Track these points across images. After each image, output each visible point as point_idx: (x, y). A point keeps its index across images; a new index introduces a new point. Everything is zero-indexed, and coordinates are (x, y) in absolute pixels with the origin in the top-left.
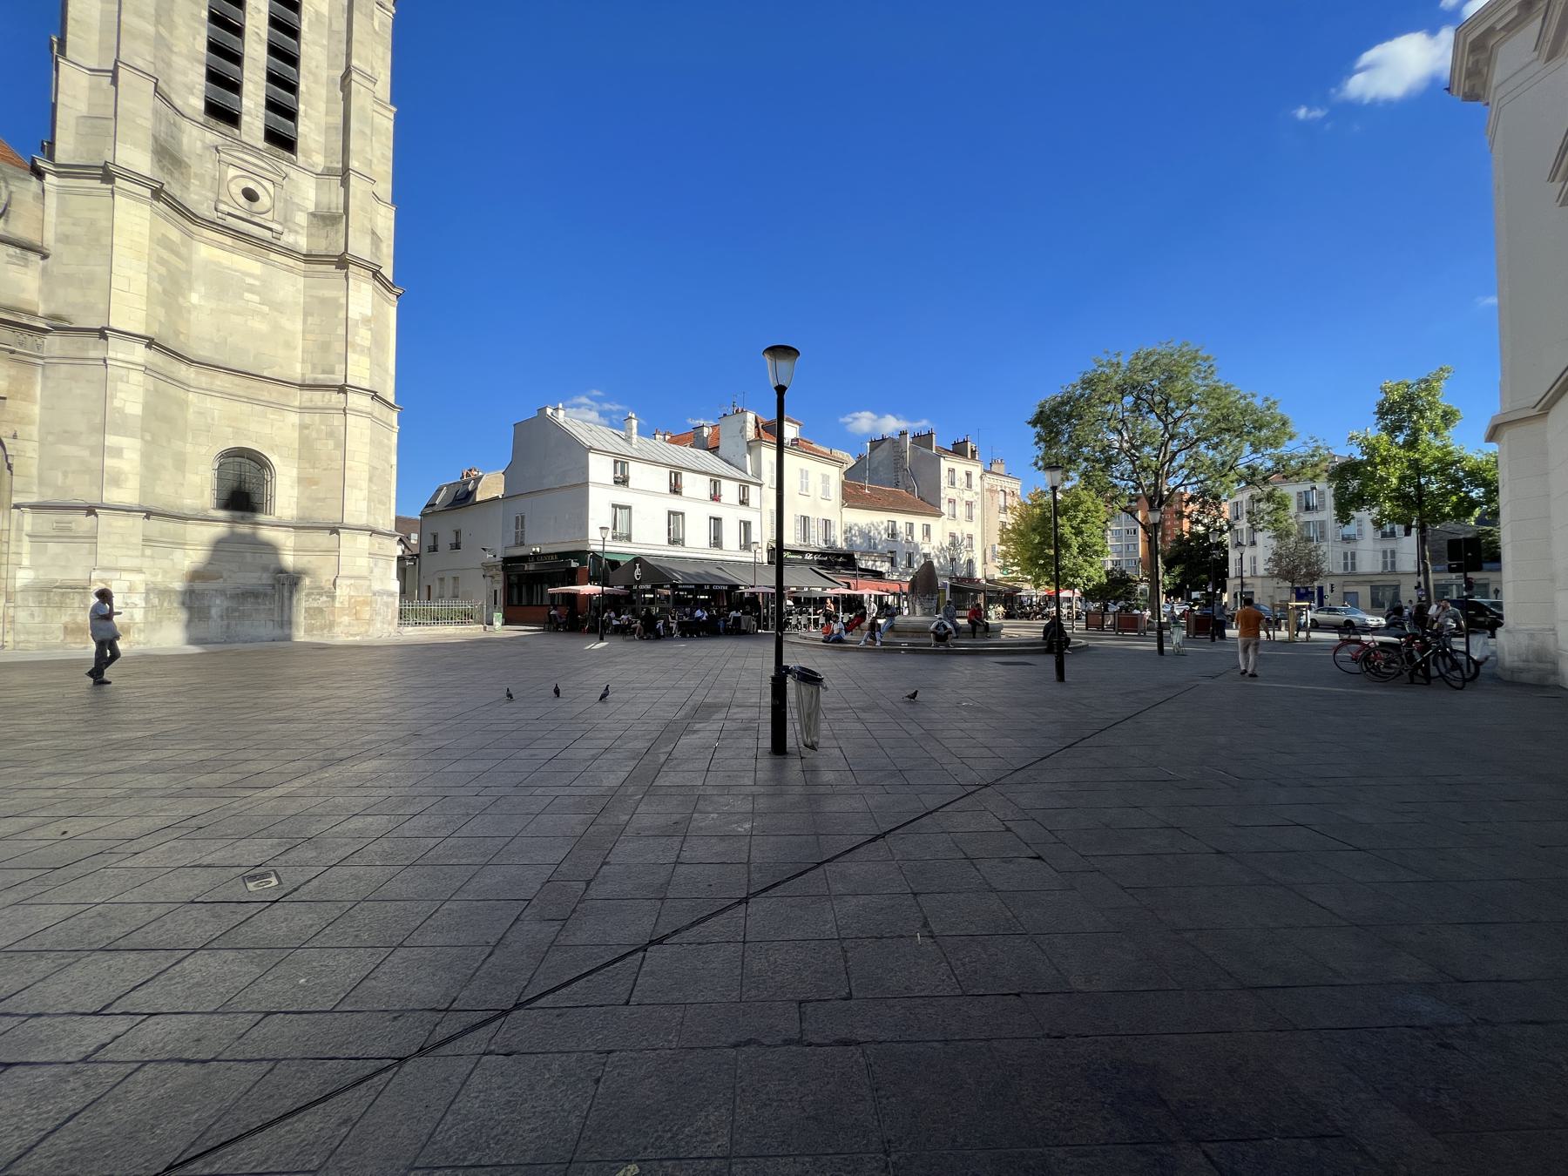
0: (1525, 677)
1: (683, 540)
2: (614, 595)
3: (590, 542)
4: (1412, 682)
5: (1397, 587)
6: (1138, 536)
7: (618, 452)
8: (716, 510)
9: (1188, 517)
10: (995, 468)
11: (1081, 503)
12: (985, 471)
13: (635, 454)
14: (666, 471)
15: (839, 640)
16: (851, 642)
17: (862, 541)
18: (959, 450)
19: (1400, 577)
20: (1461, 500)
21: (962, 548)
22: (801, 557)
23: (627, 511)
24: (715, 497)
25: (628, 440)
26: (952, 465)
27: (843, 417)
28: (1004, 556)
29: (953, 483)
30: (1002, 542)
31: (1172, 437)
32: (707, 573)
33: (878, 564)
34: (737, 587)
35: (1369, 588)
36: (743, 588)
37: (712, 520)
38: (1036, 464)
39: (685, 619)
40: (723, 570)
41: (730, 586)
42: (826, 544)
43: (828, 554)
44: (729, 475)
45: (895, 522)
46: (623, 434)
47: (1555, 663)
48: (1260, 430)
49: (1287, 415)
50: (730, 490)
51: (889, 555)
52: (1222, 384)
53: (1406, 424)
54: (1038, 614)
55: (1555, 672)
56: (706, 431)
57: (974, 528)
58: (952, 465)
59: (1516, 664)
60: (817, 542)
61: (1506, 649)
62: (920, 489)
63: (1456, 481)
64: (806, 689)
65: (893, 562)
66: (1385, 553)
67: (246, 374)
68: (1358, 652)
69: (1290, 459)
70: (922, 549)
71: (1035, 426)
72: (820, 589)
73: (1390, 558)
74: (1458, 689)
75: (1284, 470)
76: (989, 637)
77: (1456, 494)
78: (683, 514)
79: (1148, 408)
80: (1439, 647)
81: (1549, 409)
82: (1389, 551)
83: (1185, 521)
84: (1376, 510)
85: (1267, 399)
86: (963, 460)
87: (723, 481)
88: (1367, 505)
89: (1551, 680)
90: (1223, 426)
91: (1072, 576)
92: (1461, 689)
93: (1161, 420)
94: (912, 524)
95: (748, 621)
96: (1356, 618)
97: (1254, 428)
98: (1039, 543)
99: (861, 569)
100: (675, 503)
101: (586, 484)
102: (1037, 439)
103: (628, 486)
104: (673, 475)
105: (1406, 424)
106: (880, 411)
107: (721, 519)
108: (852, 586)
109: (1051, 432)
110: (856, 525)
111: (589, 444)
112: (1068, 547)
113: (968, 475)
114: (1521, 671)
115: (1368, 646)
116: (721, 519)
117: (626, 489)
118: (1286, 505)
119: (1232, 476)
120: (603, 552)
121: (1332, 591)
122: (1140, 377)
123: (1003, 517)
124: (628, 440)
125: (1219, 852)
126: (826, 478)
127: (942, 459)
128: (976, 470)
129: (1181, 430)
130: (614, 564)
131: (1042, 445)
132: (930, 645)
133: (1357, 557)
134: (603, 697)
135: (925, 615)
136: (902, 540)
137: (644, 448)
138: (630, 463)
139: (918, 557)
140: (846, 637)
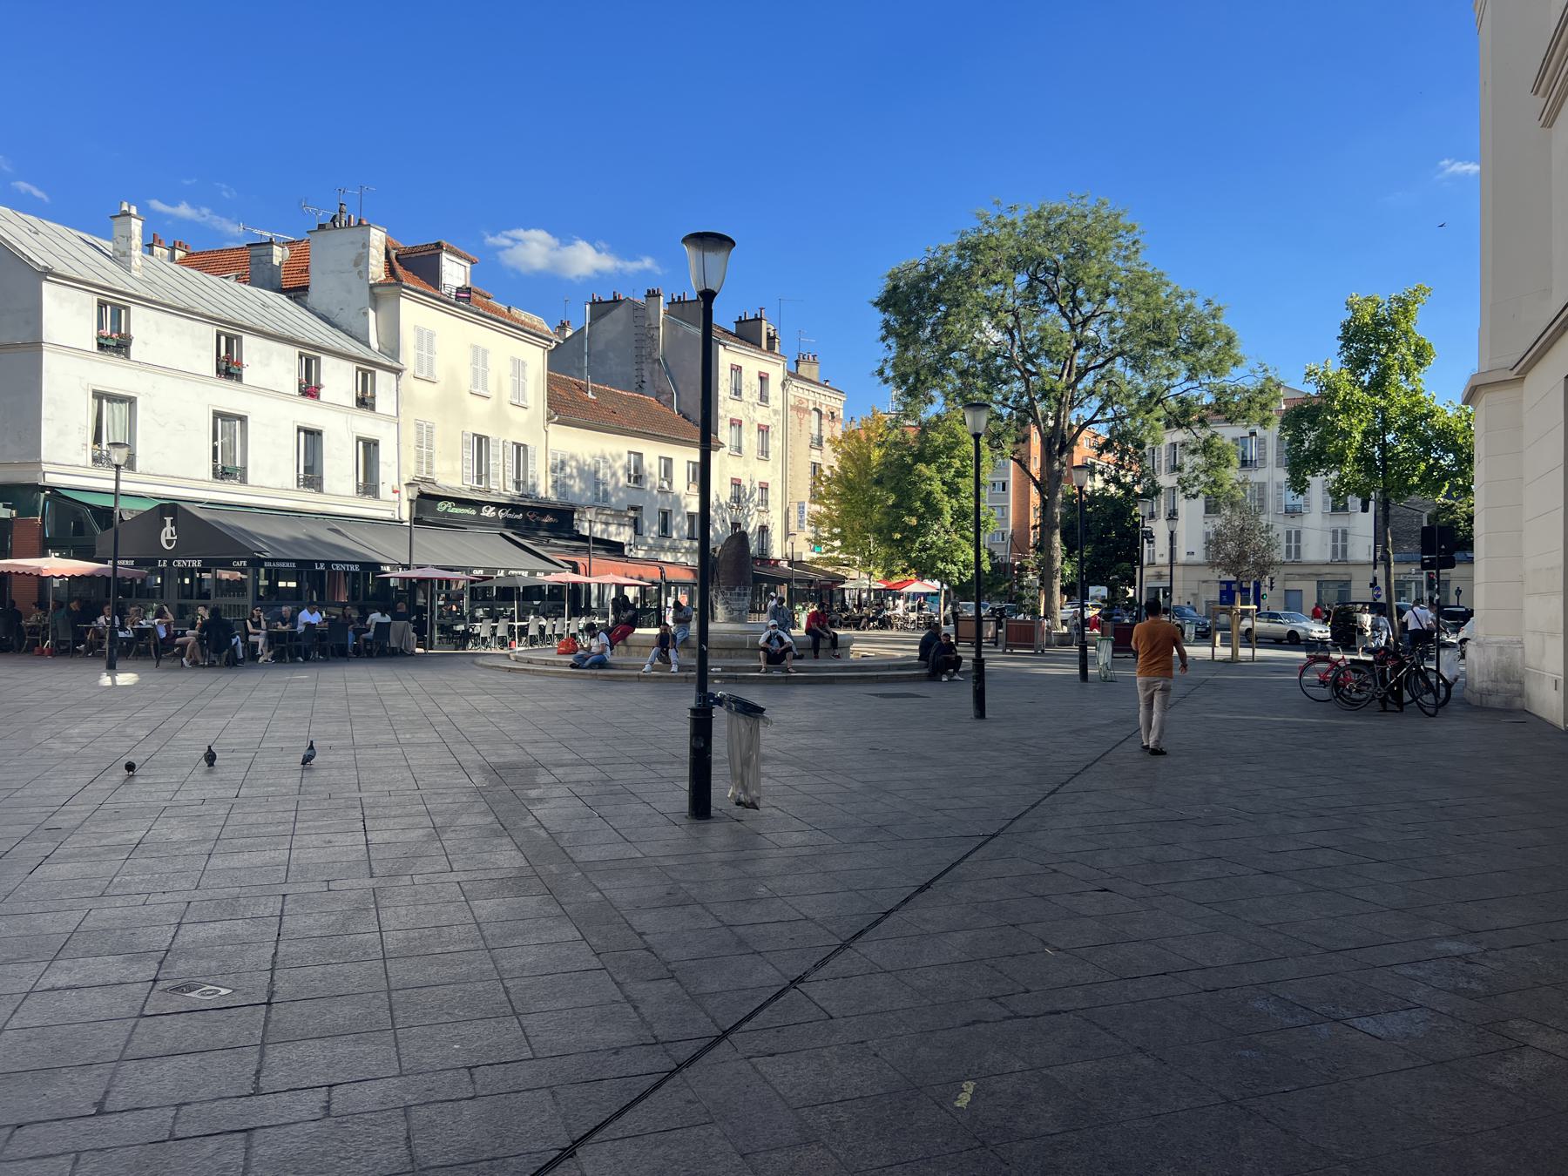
0: (1495, 701)
1: (244, 469)
2: (83, 576)
3: (45, 468)
4: (1385, 710)
5: (1347, 583)
6: (1008, 494)
7: (107, 284)
8: (309, 413)
9: (1102, 473)
10: (804, 370)
11: (958, 443)
12: (790, 374)
13: (143, 291)
14: (209, 332)
15: (601, 664)
16: (622, 667)
17: (583, 486)
18: (748, 333)
19: (1352, 570)
20: (1430, 469)
21: (751, 505)
22: (473, 512)
23: (124, 407)
24: (309, 390)
25: (121, 258)
26: (739, 360)
27: (493, 235)
28: (817, 522)
29: (738, 392)
30: (816, 497)
31: (1079, 346)
32: (316, 540)
33: (612, 529)
34: (375, 566)
35: (1315, 583)
36: (388, 569)
37: (302, 434)
38: (881, 372)
39: (281, 627)
40: (343, 535)
41: (362, 564)
42: (518, 488)
43: (524, 509)
44: (337, 347)
45: (640, 455)
46: (108, 246)
47: (1521, 683)
48: (1201, 347)
49: (1233, 329)
50: (338, 378)
51: (632, 514)
52: (1149, 270)
53: (1373, 358)
54: (873, 619)
55: (1521, 694)
56: (279, 255)
57: (767, 472)
58: (739, 360)
59: (1485, 685)
60: (502, 486)
61: (1476, 667)
62: (683, 395)
63: (1425, 442)
64: (742, 723)
65: (636, 525)
66: (1335, 532)
67: (101, 251)
68: (1327, 673)
69: (1234, 393)
70: (686, 506)
71: (885, 311)
72: (525, 574)
73: (1341, 538)
74: (1430, 716)
75: (1224, 409)
76: (838, 657)
77: (1424, 460)
78: (243, 419)
79: (1046, 294)
80: (1414, 665)
81: (1526, 373)
82: (1340, 531)
83: (1098, 477)
84: (1334, 475)
85: (1209, 303)
86: (753, 352)
87: (325, 359)
88: (1324, 467)
89: (1518, 703)
90: (1154, 337)
91: (943, 560)
92: (1433, 716)
93: (1064, 315)
94: (669, 461)
95: (402, 631)
96: (1302, 627)
97: (1194, 344)
98: (894, 506)
99: (585, 539)
100: (229, 397)
101: (35, 345)
102: (883, 332)
103: (127, 356)
104: (223, 339)
105: (1373, 358)
106: (564, 233)
107: (319, 433)
108: (582, 569)
109: (909, 322)
110: (572, 457)
111: (42, 263)
112: (937, 513)
113: (763, 378)
114: (1489, 693)
115: (1337, 665)
116: (319, 433)
117: (120, 361)
118: (1228, 461)
119: (1160, 412)
120: (116, 494)
121: (1272, 588)
122: (1041, 248)
123: (816, 456)
124: (121, 258)
125: (1266, 873)
126: (519, 365)
127: (721, 347)
128: (776, 372)
129: (1091, 334)
130: (105, 516)
131: (891, 341)
132: (758, 669)
133: (1303, 537)
134: (307, 760)
135: (732, 620)
136: (652, 488)
137: (159, 282)
138: (133, 308)
139: (679, 519)
140: (610, 657)
